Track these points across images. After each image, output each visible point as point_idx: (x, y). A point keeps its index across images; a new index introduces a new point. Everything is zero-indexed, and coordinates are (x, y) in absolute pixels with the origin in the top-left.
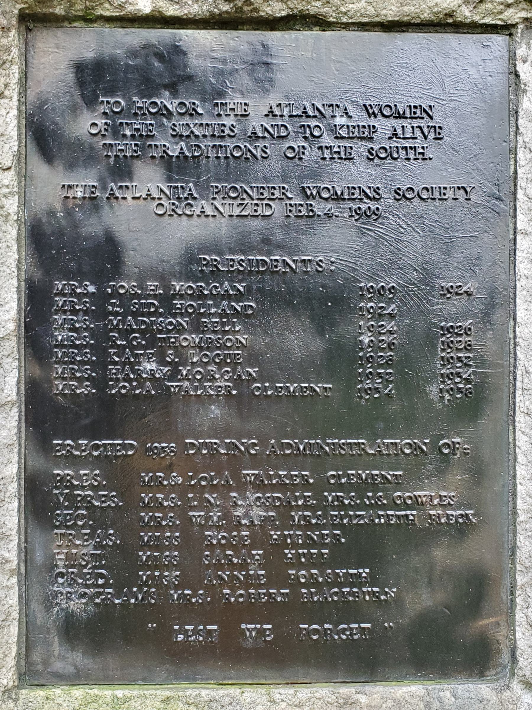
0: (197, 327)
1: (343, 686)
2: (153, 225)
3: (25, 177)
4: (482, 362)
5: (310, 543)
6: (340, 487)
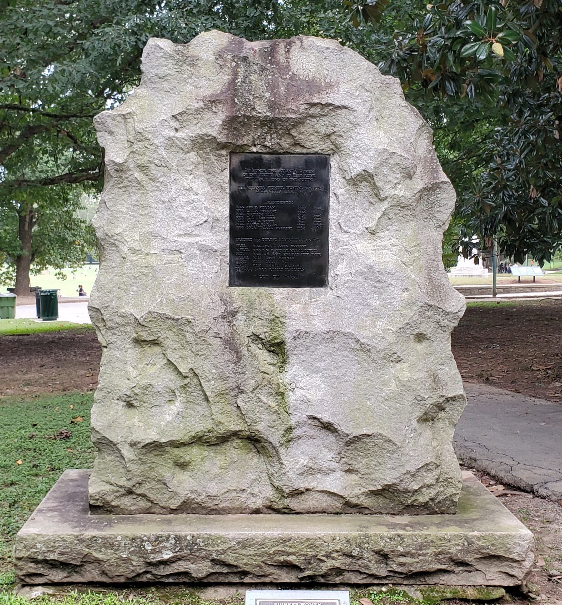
0: (265, 215)
1: (23, 331)
2: (255, 192)
3: (230, 184)
4: (322, 223)
5: (287, 259)
6: (293, 248)
